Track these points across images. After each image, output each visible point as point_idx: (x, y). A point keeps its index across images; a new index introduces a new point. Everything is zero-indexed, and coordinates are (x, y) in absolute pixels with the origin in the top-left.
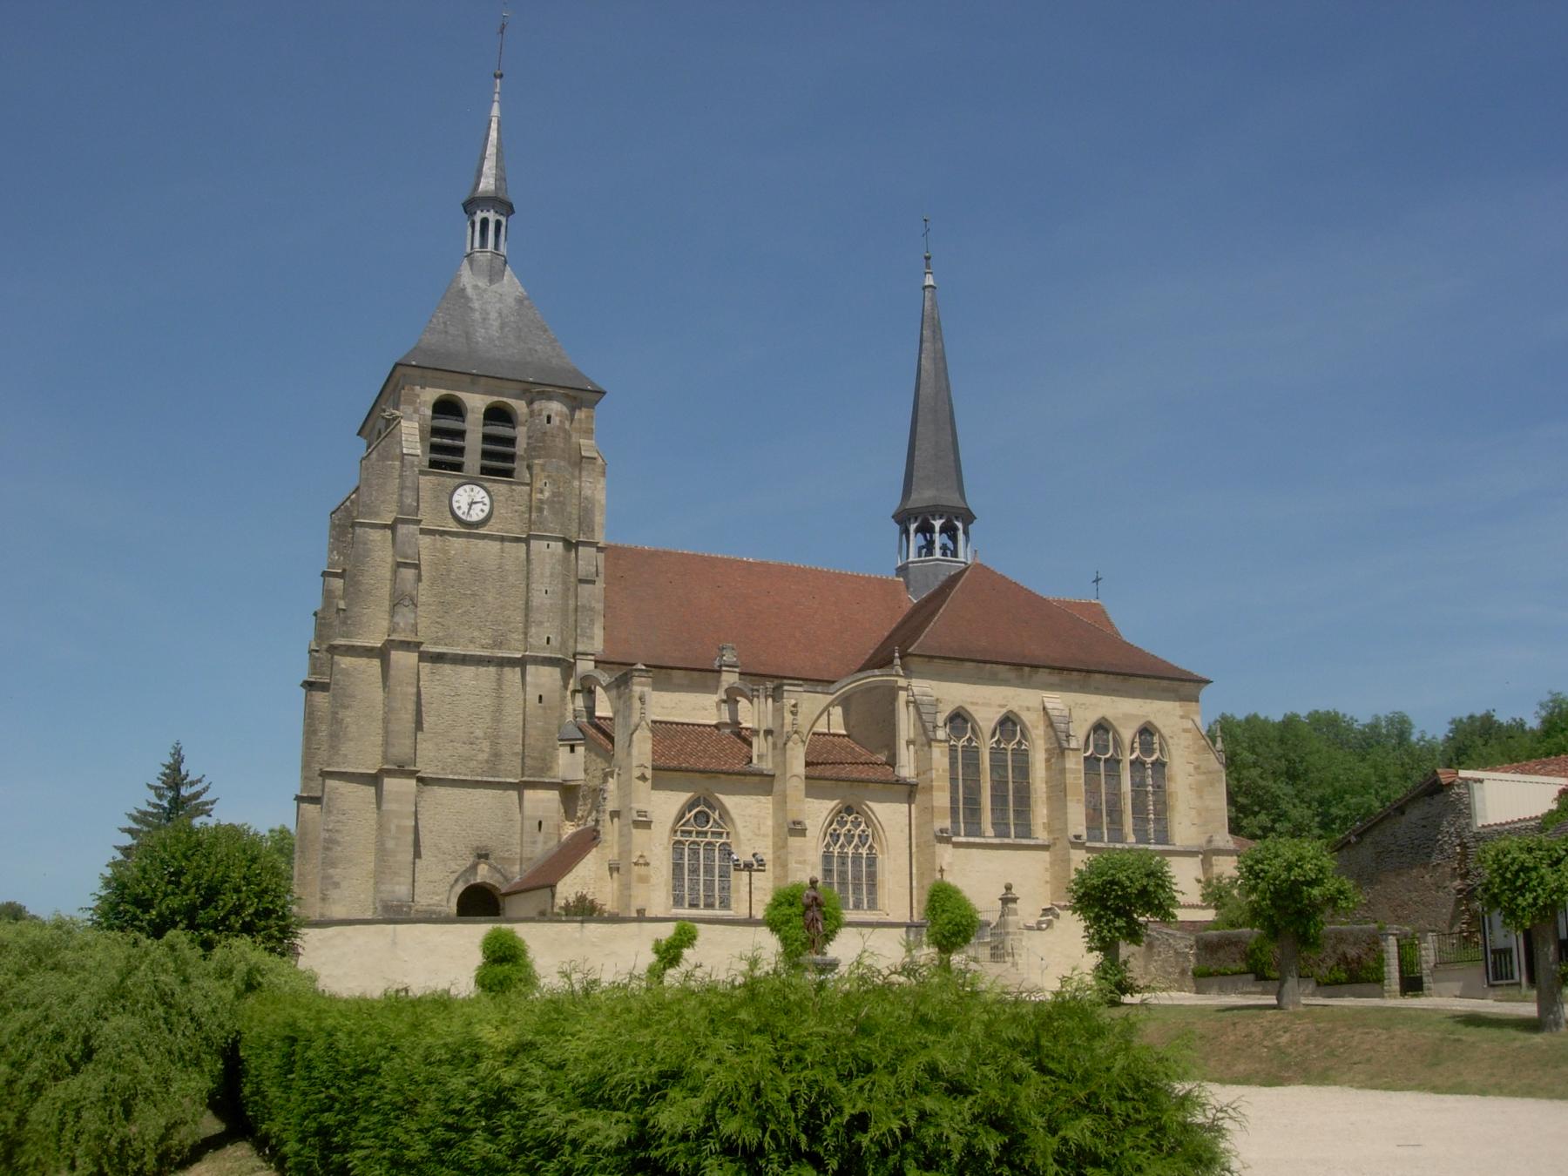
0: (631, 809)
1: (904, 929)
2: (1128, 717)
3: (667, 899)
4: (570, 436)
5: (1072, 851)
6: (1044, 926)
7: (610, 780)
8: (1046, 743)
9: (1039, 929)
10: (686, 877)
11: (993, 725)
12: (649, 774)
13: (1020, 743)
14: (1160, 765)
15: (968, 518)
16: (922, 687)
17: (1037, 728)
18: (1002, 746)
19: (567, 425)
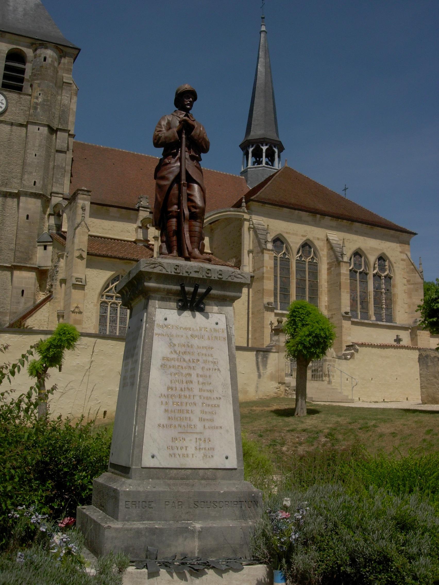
0: (72, 277)
1: (255, 353)
4: (57, 72)
5: (343, 321)
6: (349, 357)
7: (61, 260)
8: (327, 259)
9: (346, 359)
10: (108, 324)
11: (298, 246)
12: (85, 255)
13: (313, 258)
14: (389, 278)
15: (281, 149)
16: (257, 220)
17: (323, 250)
18: (303, 259)
19: (56, 64)
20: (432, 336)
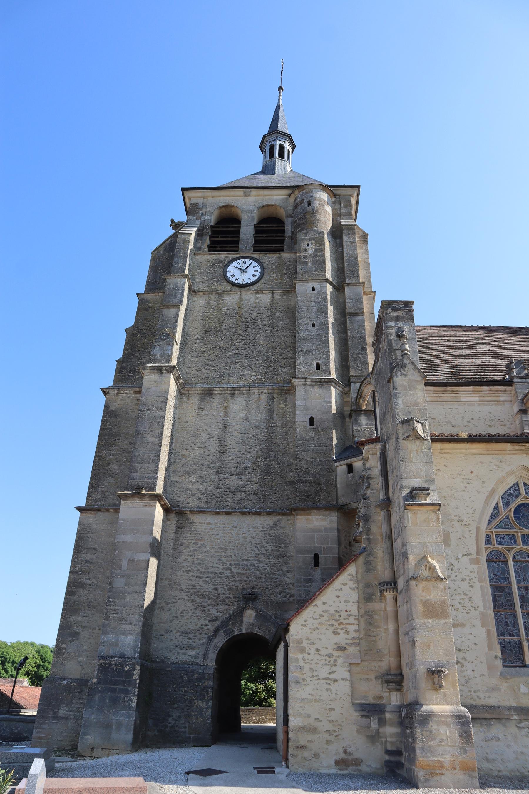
3: (490, 648)
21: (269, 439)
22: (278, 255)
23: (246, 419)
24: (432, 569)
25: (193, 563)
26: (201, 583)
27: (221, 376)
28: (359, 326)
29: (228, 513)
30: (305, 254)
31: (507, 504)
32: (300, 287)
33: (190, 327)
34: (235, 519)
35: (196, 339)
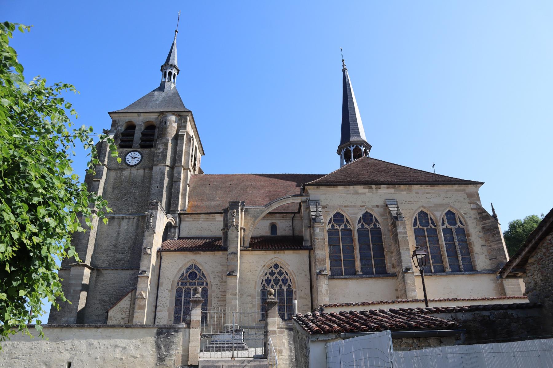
2: (438, 206)
20: (397, 347)
21: (136, 238)
22: (149, 149)
23: (127, 229)
24: (142, 295)
25: (102, 289)
26: (105, 297)
27: (119, 210)
28: (178, 187)
29: (116, 269)
30: (159, 151)
31: (187, 272)
32: (155, 168)
33: (108, 187)
34: (119, 272)
35: (110, 193)
